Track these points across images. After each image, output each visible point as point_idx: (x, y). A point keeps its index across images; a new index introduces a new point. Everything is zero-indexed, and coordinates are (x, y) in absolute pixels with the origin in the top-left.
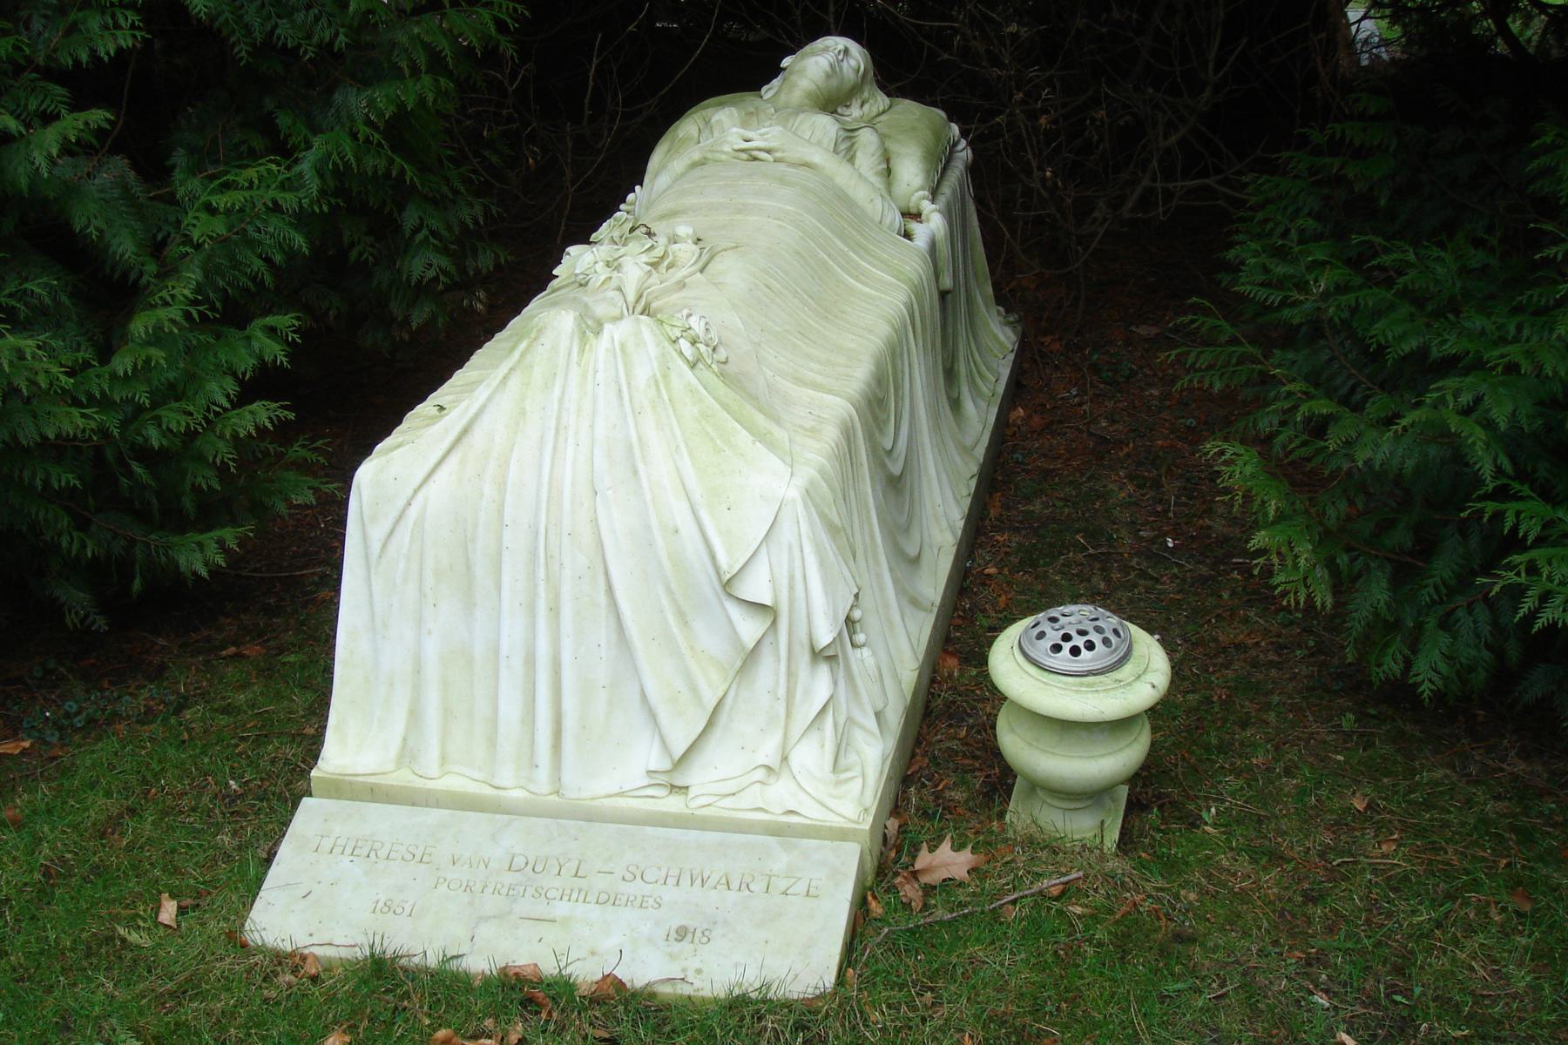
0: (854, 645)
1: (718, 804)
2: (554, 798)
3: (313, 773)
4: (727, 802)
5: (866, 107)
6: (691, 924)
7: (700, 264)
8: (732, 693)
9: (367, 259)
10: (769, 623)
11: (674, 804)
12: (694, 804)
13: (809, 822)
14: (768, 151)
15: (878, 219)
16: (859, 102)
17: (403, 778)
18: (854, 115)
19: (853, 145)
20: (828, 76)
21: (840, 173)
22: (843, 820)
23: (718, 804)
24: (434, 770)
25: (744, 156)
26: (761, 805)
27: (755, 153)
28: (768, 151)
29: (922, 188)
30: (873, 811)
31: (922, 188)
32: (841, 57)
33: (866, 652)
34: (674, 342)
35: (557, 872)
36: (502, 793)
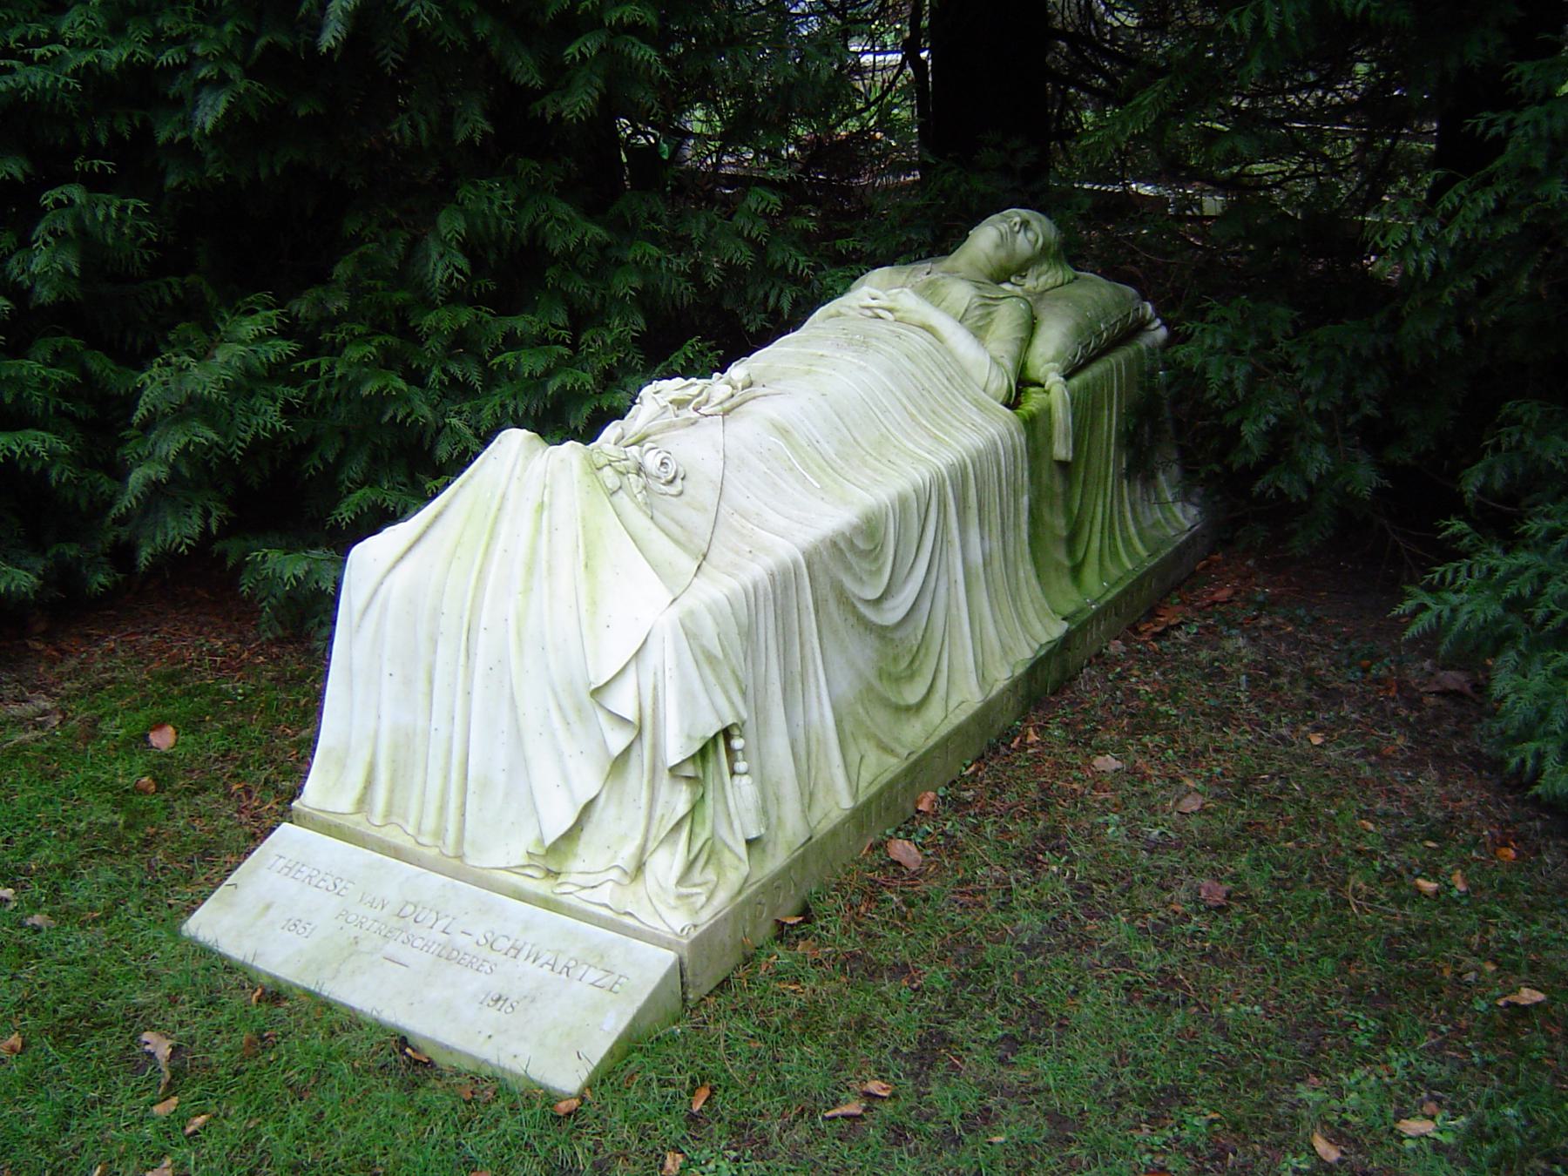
0: (733, 773)
1: (577, 894)
2: (457, 862)
3: (295, 804)
4: (585, 894)
5: (1042, 279)
6: (505, 993)
7: (727, 405)
8: (604, 792)
9: (108, 376)
10: (636, 732)
11: (543, 887)
12: (558, 890)
13: (637, 924)
14: (890, 310)
15: (982, 385)
16: (1035, 273)
17: (357, 822)
18: (1027, 286)
19: (989, 314)
20: (997, 246)
21: (960, 340)
22: (666, 929)
23: (577, 894)
24: (378, 821)
25: (869, 313)
26: (629, 910)
27: (880, 312)
28: (890, 310)
29: (1054, 360)
30: (700, 929)
31: (1054, 360)
32: (1017, 228)
33: (746, 780)
34: (598, 469)
35: (430, 924)
36: (421, 849)
